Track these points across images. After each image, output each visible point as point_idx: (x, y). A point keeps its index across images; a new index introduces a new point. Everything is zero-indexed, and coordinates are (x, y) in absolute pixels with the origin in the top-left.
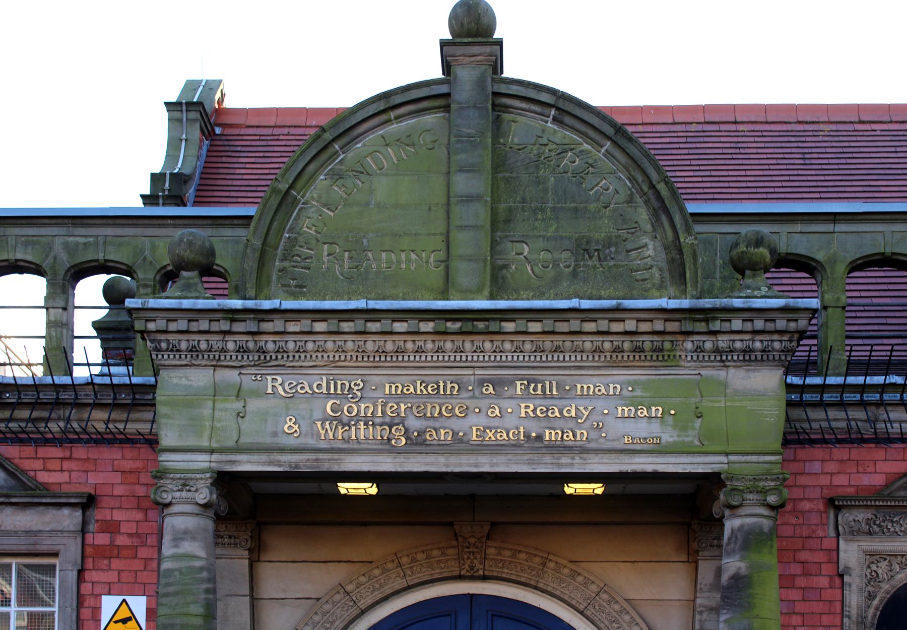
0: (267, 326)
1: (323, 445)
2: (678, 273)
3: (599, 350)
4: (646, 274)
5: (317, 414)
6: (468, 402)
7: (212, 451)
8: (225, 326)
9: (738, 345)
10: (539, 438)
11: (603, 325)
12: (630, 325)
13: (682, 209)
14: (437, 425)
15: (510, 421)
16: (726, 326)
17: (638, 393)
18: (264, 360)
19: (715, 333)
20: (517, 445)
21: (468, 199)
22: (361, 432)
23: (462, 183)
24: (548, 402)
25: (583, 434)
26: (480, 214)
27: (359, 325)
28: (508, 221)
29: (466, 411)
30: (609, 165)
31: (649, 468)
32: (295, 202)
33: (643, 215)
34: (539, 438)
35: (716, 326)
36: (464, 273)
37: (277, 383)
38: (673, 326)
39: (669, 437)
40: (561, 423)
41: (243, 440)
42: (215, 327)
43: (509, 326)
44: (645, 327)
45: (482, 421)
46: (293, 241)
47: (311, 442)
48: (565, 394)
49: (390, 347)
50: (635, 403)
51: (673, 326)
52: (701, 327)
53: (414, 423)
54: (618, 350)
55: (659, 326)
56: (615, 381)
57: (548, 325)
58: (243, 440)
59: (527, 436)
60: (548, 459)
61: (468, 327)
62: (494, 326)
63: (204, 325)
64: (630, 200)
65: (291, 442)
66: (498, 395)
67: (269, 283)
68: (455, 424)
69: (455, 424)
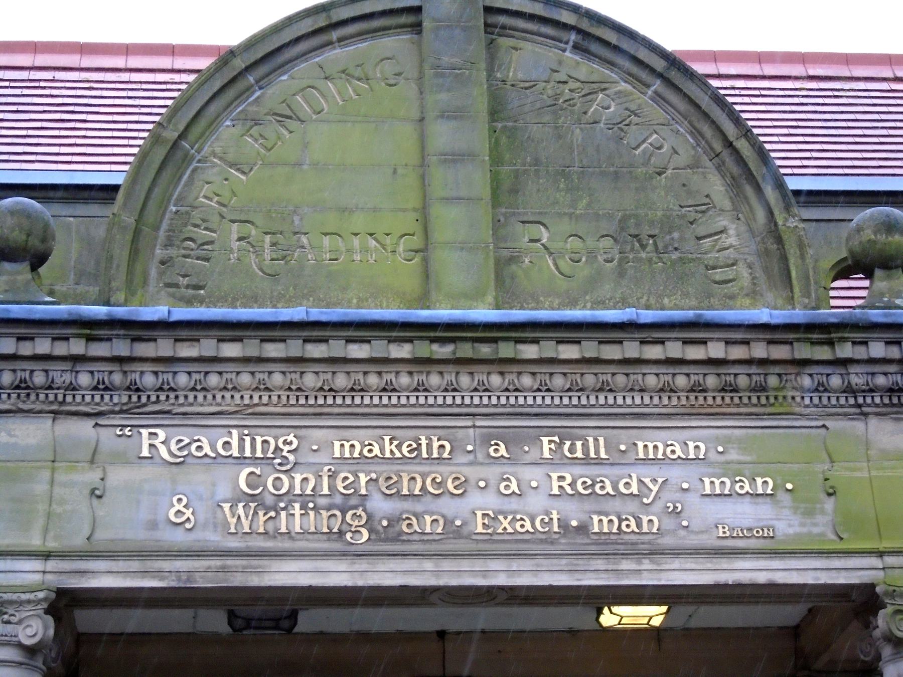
0: (145, 349)
1: (234, 543)
2: (777, 260)
3: (697, 389)
4: (729, 273)
5: (224, 491)
6: (468, 471)
7: (47, 556)
8: (77, 347)
9: (881, 381)
10: (583, 529)
11: (674, 350)
12: (716, 350)
13: (780, 185)
14: (419, 508)
15: (536, 502)
16: (860, 353)
17: (733, 456)
18: (138, 406)
19: (845, 362)
20: (548, 539)
21: (454, 158)
22: (295, 520)
23: (443, 135)
24: (594, 470)
25: (651, 522)
26: (477, 180)
27: (294, 348)
28: (514, 191)
29: (463, 484)
30: (657, 113)
31: (762, 578)
32: (187, 159)
33: (716, 187)
34: (583, 529)
35: (846, 351)
36: (453, 268)
37: (158, 440)
38: (780, 352)
39: (787, 524)
40: (617, 505)
41: (101, 535)
42: (61, 349)
43: (530, 351)
44: (738, 352)
45: (490, 501)
46: (183, 218)
47: (213, 538)
48: (619, 458)
49: (341, 381)
50: (732, 471)
51: (780, 352)
52: (823, 353)
53: (380, 506)
54: (697, 389)
55: (759, 351)
56: (694, 440)
57: (590, 349)
58: (101, 535)
59: (564, 524)
60: (600, 564)
61: (466, 350)
62: (506, 350)
63: (43, 346)
64: (695, 165)
65: (179, 538)
66: (509, 460)
67: (145, 282)
68: (447, 506)
69: (447, 506)
